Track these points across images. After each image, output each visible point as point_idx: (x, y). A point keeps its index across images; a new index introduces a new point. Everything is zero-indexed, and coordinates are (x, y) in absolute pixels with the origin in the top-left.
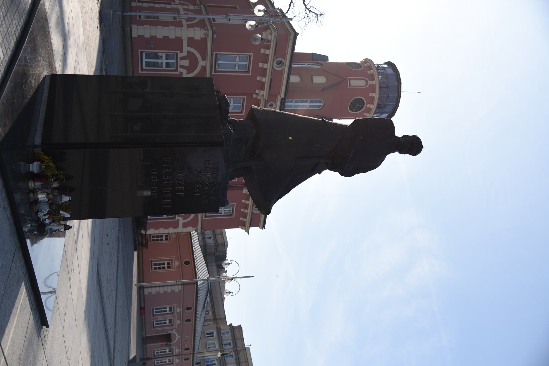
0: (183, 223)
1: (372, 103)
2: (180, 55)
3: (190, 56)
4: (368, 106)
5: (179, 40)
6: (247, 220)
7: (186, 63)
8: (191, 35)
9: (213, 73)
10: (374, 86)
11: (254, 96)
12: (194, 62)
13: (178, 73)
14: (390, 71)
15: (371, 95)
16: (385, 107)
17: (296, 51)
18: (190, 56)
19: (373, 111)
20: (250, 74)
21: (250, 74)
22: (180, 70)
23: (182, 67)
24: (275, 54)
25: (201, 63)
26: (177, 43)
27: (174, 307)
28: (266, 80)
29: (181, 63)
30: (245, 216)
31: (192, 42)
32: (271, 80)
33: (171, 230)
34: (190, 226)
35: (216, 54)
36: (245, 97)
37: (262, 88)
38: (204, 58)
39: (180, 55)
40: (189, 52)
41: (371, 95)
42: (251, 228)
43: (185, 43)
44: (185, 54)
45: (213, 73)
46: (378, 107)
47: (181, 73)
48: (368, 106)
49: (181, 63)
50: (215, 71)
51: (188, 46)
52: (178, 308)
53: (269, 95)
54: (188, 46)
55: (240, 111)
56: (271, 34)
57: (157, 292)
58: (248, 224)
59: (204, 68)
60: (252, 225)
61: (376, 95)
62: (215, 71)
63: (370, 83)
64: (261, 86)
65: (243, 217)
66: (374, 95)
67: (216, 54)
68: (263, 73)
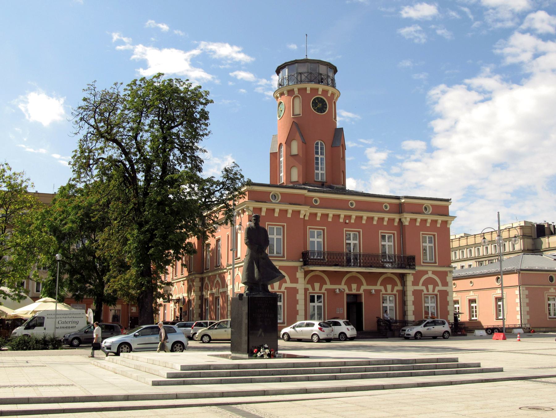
0: (443, 286)
1: (317, 90)
2: (425, 292)
3: (425, 284)
4: (320, 93)
5: (415, 293)
6: (440, 219)
7: (431, 287)
8: (411, 284)
9: (285, 259)
10: (299, 90)
11: (307, 218)
12: (430, 281)
13: (286, 291)
14: (286, 72)
15: (308, 92)
16: (321, 74)
17: (268, 182)
18: (425, 284)
19: (326, 88)
20: (285, 224)
21: (285, 224)
22: (395, 292)
23: (392, 291)
24: (265, 202)
25: (430, 275)
26: (417, 294)
27: (548, 295)
28: (291, 208)
29: (431, 291)
30: (434, 222)
31: (415, 283)
32: (291, 204)
33: (300, 297)
34: (446, 279)
35: (423, 262)
36: (308, 227)
37: (299, 212)
38: (426, 272)
39: (425, 292)
40: (423, 285)
41: (308, 92)
42: (450, 214)
43: (416, 288)
44: (424, 288)
45: (285, 259)
46: (321, 81)
47: (397, 291)
48: (320, 93)
49: (431, 291)
50: (435, 263)
51: (418, 285)
52: (550, 291)
53: (305, 204)
54: (418, 285)
55: (357, 233)
56: (406, 218)
57: (528, 314)
58: (444, 218)
59: (434, 273)
60: (447, 214)
61: (309, 86)
62: (283, 257)
63: (296, 92)
64: (371, 219)
65: (383, 221)
66: (308, 89)
67: (423, 262)
68: (434, 222)
